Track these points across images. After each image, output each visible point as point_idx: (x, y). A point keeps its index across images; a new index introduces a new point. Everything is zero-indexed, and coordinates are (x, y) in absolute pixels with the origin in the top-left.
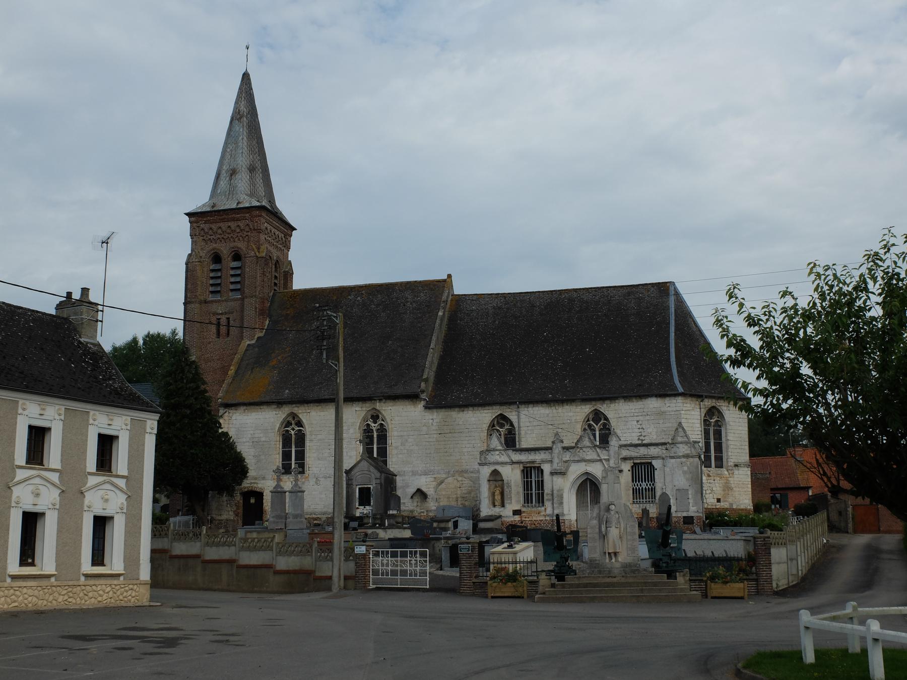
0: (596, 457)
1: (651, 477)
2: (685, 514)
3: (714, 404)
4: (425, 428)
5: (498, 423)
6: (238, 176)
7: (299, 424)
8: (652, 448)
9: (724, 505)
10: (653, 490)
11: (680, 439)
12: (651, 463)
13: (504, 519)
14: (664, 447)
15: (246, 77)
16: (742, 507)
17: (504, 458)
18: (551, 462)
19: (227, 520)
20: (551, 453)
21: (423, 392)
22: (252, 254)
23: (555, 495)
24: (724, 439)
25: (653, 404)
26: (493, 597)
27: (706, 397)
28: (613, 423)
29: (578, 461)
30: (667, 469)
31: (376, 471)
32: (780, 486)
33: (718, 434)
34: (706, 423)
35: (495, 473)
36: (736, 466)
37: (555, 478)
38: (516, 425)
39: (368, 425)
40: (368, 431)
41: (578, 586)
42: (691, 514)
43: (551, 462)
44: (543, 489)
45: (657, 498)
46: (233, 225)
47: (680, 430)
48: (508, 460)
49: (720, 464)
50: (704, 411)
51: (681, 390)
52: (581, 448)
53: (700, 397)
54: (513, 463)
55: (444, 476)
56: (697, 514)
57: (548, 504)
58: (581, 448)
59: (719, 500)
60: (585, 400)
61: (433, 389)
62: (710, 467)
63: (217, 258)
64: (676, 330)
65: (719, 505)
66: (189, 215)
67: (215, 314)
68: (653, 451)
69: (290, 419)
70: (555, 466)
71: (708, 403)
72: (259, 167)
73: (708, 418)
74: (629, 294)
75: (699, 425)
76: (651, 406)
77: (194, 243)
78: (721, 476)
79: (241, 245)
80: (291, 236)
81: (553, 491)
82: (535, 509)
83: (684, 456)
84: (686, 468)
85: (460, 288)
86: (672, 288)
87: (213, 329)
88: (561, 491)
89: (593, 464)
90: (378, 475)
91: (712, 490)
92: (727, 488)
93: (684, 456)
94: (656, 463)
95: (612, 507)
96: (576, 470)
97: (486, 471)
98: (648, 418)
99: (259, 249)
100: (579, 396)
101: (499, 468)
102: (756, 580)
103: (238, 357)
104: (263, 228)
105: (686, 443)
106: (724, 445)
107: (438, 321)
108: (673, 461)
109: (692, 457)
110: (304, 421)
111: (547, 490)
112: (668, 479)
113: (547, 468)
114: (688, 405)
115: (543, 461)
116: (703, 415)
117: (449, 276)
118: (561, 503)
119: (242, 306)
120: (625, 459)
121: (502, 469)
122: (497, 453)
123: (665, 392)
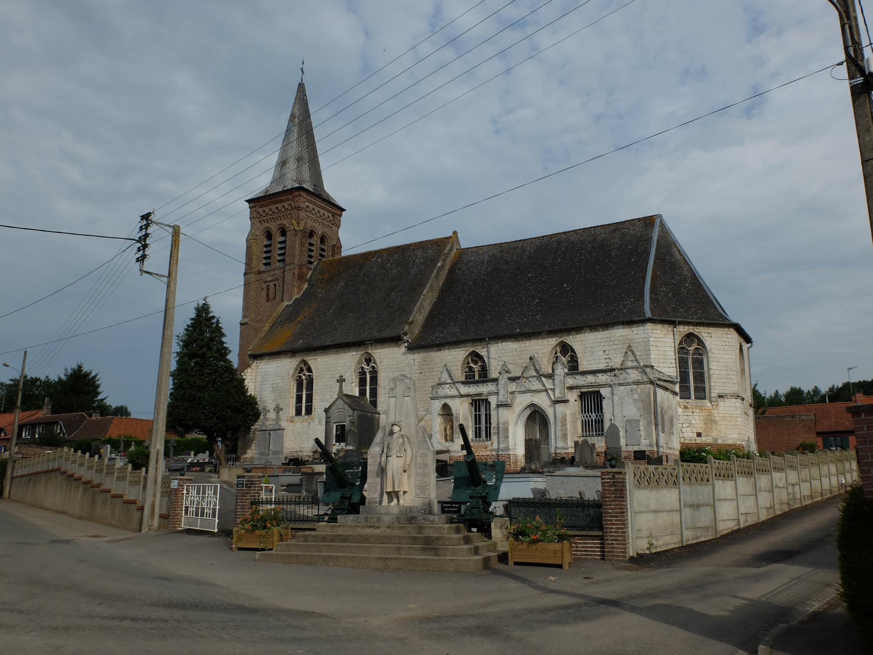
0: (541, 387)
1: (599, 409)
2: (636, 448)
3: (690, 331)
4: (408, 369)
5: (472, 360)
6: (287, 166)
7: (309, 370)
8: (600, 375)
9: (705, 440)
10: (601, 422)
11: (630, 364)
12: (599, 392)
13: (452, 454)
14: (612, 374)
15: (301, 87)
16: (730, 442)
17: (454, 392)
18: (497, 393)
19: (252, 458)
20: (497, 385)
21: (406, 334)
22: (292, 228)
23: (501, 428)
24: (706, 368)
25: (620, 332)
26: (240, 549)
27: (680, 323)
28: (579, 355)
29: (524, 392)
30: (616, 398)
31: (349, 409)
32: (840, 430)
33: (699, 364)
34: (681, 350)
35: (446, 407)
36: (720, 396)
37: (501, 410)
38: (486, 359)
39: (362, 368)
40: (363, 373)
41: (334, 538)
42: (643, 448)
43: (497, 393)
44: (490, 424)
45: (605, 431)
46: (279, 206)
47: (630, 353)
48: (457, 394)
49: (701, 393)
50: (678, 339)
51: (648, 314)
52: (527, 378)
53: (673, 323)
54: (462, 396)
55: (424, 413)
56: (650, 448)
57: (494, 437)
58: (527, 378)
59: (699, 435)
60: (551, 333)
61: (421, 332)
62: (690, 398)
63: (269, 236)
64: (656, 259)
65: (699, 440)
66: (249, 201)
67: (266, 282)
68: (602, 378)
69: (302, 365)
70: (501, 398)
71: (684, 330)
72: (310, 157)
73: (685, 345)
74: (615, 231)
75: (673, 353)
76: (618, 334)
77: (252, 224)
78: (702, 408)
79: (285, 222)
80: (341, 216)
81: (498, 424)
82: (482, 444)
83: (634, 383)
84: (636, 396)
85: (465, 243)
86: (658, 221)
87: (265, 295)
88: (506, 423)
89: (537, 395)
90: (351, 412)
91: (690, 423)
92: (710, 421)
93: (634, 383)
94: (604, 392)
95: (396, 429)
96: (522, 401)
97: (437, 405)
98: (615, 347)
99: (298, 223)
100: (546, 328)
101: (449, 402)
102: (601, 538)
103: (275, 315)
104: (302, 205)
105: (636, 368)
106: (706, 375)
107: (435, 271)
108: (622, 388)
109: (643, 383)
110: (312, 367)
111: (494, 424)
112: (617, 409)
113: (493, 400)
114: (658, 332)
115: (490, 394)
116: (677, 342)
117: (455, 233)
118: (507, 437)
119: (284, 273)
120: (571, 388)
121: (452, 403)
122: (448, 386)
123: (634, 320)
